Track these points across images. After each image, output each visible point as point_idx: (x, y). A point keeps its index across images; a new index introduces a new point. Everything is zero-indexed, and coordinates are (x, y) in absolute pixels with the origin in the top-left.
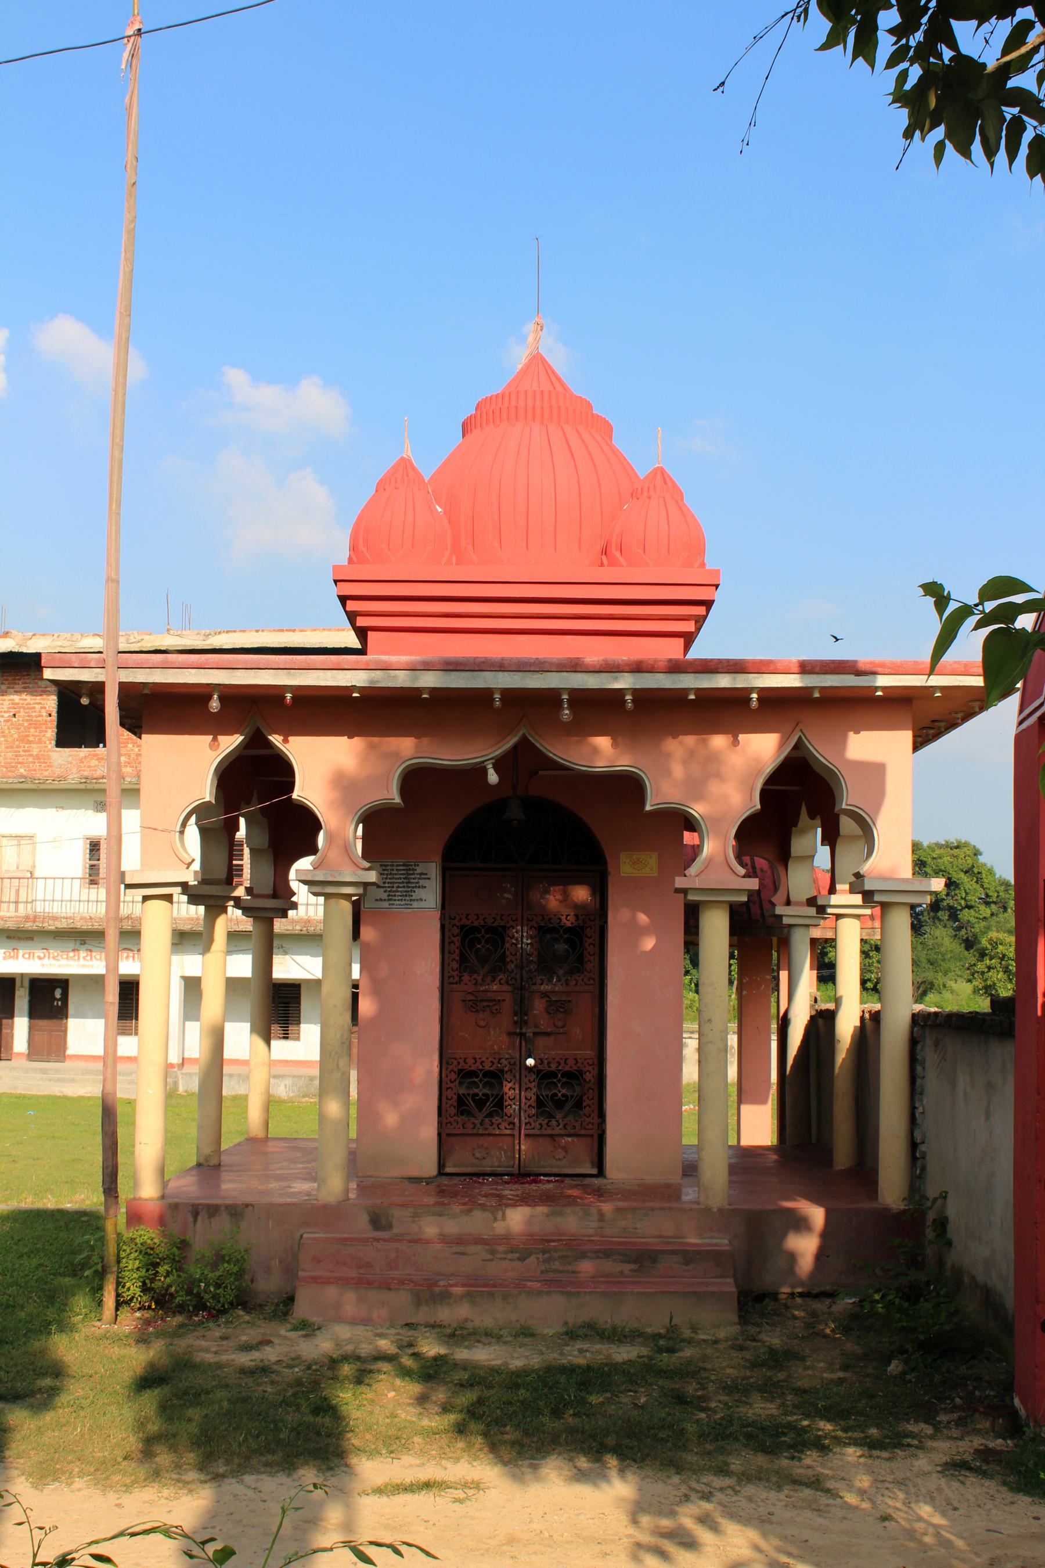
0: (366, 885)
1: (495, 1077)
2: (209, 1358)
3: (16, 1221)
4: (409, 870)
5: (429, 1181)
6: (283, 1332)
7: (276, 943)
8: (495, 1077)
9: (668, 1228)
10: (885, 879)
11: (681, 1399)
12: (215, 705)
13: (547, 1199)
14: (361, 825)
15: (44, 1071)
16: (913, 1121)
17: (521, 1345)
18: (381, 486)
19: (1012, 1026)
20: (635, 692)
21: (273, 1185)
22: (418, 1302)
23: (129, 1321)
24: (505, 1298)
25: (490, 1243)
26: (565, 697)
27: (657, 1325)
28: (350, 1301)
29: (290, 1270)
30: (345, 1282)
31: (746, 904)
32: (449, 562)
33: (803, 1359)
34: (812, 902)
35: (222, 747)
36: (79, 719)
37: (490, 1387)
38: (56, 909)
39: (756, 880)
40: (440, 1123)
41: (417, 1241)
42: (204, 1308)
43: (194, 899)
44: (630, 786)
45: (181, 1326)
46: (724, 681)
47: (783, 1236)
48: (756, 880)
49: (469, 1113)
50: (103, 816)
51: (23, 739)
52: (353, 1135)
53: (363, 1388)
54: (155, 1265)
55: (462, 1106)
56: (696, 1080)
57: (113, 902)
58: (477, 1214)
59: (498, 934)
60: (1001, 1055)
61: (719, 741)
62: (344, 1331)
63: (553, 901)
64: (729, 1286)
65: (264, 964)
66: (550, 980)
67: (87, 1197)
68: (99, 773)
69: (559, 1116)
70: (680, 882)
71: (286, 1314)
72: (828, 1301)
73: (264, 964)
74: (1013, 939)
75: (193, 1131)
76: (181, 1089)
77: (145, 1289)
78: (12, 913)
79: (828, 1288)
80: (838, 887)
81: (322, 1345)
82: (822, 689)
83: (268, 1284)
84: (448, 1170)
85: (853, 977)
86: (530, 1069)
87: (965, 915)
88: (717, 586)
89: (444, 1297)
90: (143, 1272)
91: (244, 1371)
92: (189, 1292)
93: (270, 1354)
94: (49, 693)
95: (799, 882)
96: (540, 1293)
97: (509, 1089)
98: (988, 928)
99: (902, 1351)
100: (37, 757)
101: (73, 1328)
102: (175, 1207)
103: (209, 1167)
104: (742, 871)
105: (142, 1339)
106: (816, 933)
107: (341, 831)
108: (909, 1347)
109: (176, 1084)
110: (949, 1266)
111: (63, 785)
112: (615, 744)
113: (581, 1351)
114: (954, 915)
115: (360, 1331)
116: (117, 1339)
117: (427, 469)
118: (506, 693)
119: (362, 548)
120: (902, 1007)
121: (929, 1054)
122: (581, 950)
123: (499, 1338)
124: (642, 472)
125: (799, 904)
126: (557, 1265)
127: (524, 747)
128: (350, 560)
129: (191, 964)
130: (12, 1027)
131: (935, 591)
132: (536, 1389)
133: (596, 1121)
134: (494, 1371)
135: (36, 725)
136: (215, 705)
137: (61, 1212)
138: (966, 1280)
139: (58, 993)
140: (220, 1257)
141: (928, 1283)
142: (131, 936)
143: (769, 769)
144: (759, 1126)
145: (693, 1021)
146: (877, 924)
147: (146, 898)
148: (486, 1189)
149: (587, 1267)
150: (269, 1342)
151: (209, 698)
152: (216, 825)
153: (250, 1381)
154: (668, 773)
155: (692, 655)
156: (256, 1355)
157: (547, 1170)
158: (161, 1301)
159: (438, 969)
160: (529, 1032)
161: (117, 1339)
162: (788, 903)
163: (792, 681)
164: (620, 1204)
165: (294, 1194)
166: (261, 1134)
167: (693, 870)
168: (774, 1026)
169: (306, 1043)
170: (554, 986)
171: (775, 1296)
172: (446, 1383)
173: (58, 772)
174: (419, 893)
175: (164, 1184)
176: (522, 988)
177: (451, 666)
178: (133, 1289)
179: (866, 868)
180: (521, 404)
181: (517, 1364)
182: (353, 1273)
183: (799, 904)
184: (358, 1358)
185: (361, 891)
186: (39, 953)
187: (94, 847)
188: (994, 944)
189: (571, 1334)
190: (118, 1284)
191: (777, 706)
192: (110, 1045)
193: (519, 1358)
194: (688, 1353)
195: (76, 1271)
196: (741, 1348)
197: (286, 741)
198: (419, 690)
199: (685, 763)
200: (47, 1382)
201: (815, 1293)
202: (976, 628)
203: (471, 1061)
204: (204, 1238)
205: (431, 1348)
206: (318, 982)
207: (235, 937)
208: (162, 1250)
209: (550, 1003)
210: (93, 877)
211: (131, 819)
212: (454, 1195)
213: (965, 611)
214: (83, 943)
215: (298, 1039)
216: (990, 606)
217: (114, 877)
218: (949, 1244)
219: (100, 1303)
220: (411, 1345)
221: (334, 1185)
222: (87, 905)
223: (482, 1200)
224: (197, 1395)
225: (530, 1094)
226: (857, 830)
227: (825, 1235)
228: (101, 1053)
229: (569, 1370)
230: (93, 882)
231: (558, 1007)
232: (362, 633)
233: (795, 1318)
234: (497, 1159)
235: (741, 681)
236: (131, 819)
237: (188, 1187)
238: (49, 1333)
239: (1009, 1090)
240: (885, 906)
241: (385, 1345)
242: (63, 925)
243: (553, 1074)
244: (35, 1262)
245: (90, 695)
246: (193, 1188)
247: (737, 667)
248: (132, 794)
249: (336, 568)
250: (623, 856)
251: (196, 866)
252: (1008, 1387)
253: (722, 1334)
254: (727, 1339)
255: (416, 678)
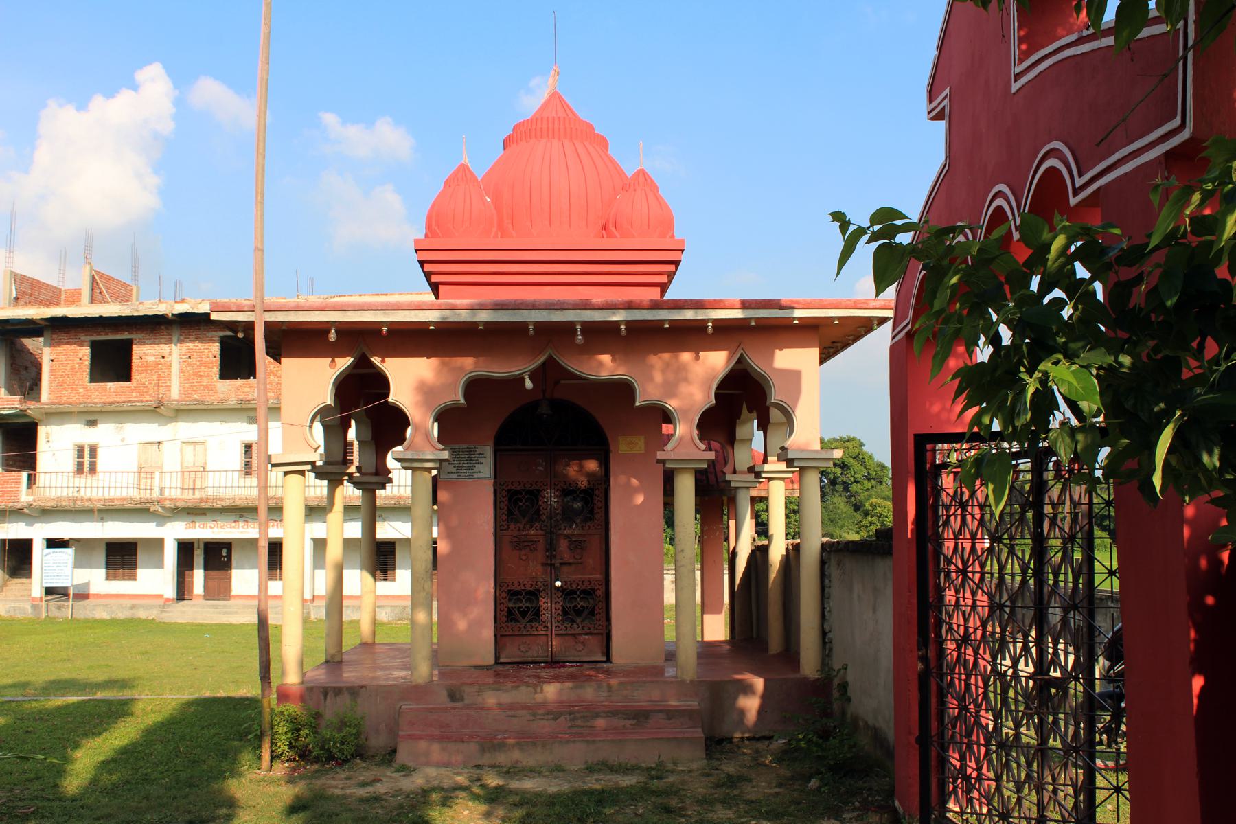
0: (441, 461)
1: (533, 595)
2: (337, 792)
3: (198, 705)
4: (471, 451)
5: (488, 668)
6: (389, 773)
7: (378, 513)
8: (533, 595)
9: (656, 694)
10: (803, 451)
11: (668, 810)
12: (333, 336)
13: (571, 677)
14: (436, 425)
15: (216, 607)
16: (823, 617)
17: (556, 778)
18: (447, 184)
19: (890, 547)
20: (627, 323)
21: (379, 673)
22: (483, 750)
23: (281, 769)
24: (544, 746)
25: (534, 710)
26: (579, 327)
27: (649, 760)
28: (436, 751)
29: (393, 731)
30: (432, 738)
31: (706, 469)
32: (496, 236)
33: (750, 781)
34: (751, 470)
35: (338, 366)
36: (237, 359)
37: (535, 805)
38: (222, 493)
39: (713, 453)
40: (496, 628)
41: (482, 708)
42: (333, 758)
43: (320, 475)
44: (624, 389)
45: (317, 771)
46: (689, 315)
47: (736, 698)
48: (713, 453)
49: (516, 620)
50: (255, 427)
51: (197, 374)
52: (435, 640)
53: (446, 809)
54: (298, 730)
55: (511, 616)
56: (675, 601)
57: (263, 486)
58: (523, 688)
59: (534, 495)
60: (884, 567)
61: (686, 357)
62: (432, 772)
63: (572, 471)
64: (699, 733)
65: (370, 528)
66: (571, 527)
67: (250, 689)
68: (250, 397)
69: (578, 620)
70: (660, 455)
71: (391, 761)
72: (767, 742)
73: (370, 528)
74: (889, 504)
75: (322, 645)
76: (313, 617)
77: (291, 747)
78: (191, 496)
79: (767, 733)
80: (769, 458)
81: (417, 781)
82: (757, 319)
83: (377, 741)
84: (502, 660)
85: (781, 517)
86: (558, 589)
87: (854, 488)
88: (682, 251)
89: (501, 746)
90: (289, 735)
91: (362, 800)
92: (322, 748)
93: (380, 788)
94: (214, 341)
95: (741, 457)
96: (568, 742)
97: (544, 603)
98: (870, 496)
99: (818, 772)
100: (206, 387)
101: (241, 775)
102: (310, 689)
103: (334, 662)
104: (703, 447)
105: (291, 780)
106: (754, 493)
107: (423, 427)
108: (823, 770)
109: (309, 613)
110: (849, 716)
111: (225, 406)
112: (614, 360)
113: (597, 780)
114: (846, 488)
115: (443, 771)
116: (272, 781)
117: (479, 171)
118: (538, 325)
119: (434, 227)
120: (814, 540)
121: (833, 570)
122: (592, 504)
123: (540, 773)
124: (630, 172)
125: (742, 473)
126: (579, 723)
127: (550, 363)
128: (426, 235)
129: (318, 529)
130: (192, 577)
131: (838, 217)
132: (567, 806)
133: (605, 623)
134: (537, 794)
135: (204, 363)
136: (333, 336)
137: (230, 698)
138: (861, 723)
139: (224, 552)
140: (343, 724)
141: (835, 728)
142: (276, 511)
143: (721, 376)
144: (716, 628)
145: (669, 563)
146: (796, 486)
147: (286, 473)
148: (529, 672)
149: (601, 722)
150: (379, 780)
151: (329, 331)
152: (332, 423)
153: (367, 807)
154: (651, 379)
155: (667, 297)
156: (370, 789)
157: (571, 659)
158: (304, 755)
159: (492, 521)
160: (557, 563)
161: (272, 781)
162: (735, 472)
163: (737, 314)
164: (622, 679)
165: (395, 679)
166: (370, 641)
167: (669, 446)
168: (726, 556)
169: (402, 582)
170: (574, 530)
171: (730, 740)
172: (504, 804)
173: (221, 396)
174: (478, 468)
175: (303, 675)
176: (551, 533)
177: (499, 306)
178: (283, 746)
179: (788, 444)
180: (545, 126)
181: (553, 789)
182: (437, 732)
183: (742, 473)
184: (443, 789)
185: (437, 465)
186: (211, 524)
187: (248, 448)
188: (874, 506)
189: (590, 769)
190: (272, 743)
191: (726, 332)
192: (263, 588)
193: (554, 786)
194: (671, 779)
195: (242, 736)
196: (708, 775)
197: (383, 361)
198: (476, 324)
199: (663, 371)
200: (224, 811)
201: (759, 737)
202: (868, 242)
203: (516, 584)
204: (332, 710)
205: (493, 781)
206: (408, 540)
207: (350, 511)
208: (303, 719)
209: (571, 542)
210: (248, 468)
211: (275, 428)
212: (506, 677)
213: (861, 231)
214: (241, 516)
215: (394, 580)
216: (877, 228)
217: (263, 458)
218: (849, 700)
219: (260, 757)
220: (479, 780)
221: (423, 670)
222: (244, 490)
223: (527, 680)
224: (330, 816)
225: (558, 606)
226: (782, 418)
227: (764, 697)
228: (256, 593)
229: (590, 793)
230: (247, 474)
231: (577, 545)
232: (435, 288)
233: (744, 754)
234: (536, 651)
235: (701, 315)
236: (275, 428)
237: (320, 676)
238: (224, 778)
239: (889, 591)
240: (802, 469)
241: (461, 779)
242: (227, 504)
243: (574, 592)
244: (212, 732)
245: (244, 331)
246: (323, 677)
247: (698, 305)
248: (275, 410)
249: (416, 241)
250: (620, 439)
251: (322, 450)
252: (891, 794)
253: (694, 766)
254: (698, 769)
255: (475, 315)
